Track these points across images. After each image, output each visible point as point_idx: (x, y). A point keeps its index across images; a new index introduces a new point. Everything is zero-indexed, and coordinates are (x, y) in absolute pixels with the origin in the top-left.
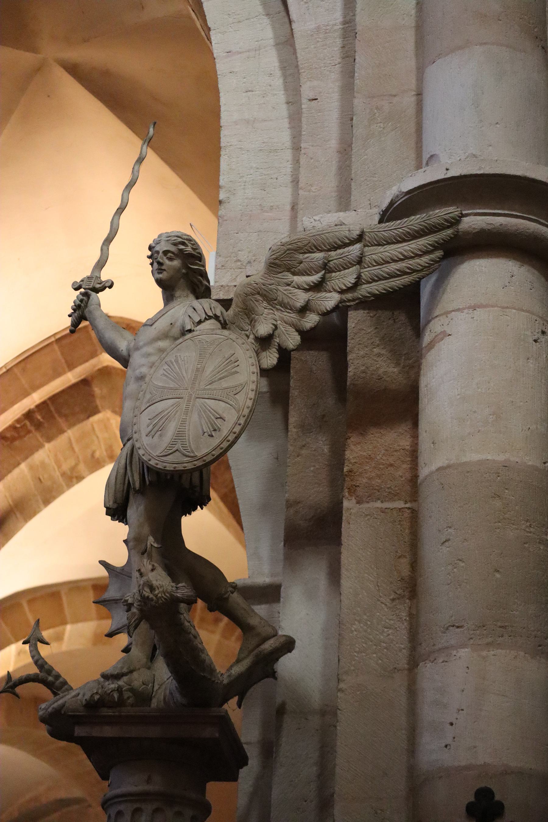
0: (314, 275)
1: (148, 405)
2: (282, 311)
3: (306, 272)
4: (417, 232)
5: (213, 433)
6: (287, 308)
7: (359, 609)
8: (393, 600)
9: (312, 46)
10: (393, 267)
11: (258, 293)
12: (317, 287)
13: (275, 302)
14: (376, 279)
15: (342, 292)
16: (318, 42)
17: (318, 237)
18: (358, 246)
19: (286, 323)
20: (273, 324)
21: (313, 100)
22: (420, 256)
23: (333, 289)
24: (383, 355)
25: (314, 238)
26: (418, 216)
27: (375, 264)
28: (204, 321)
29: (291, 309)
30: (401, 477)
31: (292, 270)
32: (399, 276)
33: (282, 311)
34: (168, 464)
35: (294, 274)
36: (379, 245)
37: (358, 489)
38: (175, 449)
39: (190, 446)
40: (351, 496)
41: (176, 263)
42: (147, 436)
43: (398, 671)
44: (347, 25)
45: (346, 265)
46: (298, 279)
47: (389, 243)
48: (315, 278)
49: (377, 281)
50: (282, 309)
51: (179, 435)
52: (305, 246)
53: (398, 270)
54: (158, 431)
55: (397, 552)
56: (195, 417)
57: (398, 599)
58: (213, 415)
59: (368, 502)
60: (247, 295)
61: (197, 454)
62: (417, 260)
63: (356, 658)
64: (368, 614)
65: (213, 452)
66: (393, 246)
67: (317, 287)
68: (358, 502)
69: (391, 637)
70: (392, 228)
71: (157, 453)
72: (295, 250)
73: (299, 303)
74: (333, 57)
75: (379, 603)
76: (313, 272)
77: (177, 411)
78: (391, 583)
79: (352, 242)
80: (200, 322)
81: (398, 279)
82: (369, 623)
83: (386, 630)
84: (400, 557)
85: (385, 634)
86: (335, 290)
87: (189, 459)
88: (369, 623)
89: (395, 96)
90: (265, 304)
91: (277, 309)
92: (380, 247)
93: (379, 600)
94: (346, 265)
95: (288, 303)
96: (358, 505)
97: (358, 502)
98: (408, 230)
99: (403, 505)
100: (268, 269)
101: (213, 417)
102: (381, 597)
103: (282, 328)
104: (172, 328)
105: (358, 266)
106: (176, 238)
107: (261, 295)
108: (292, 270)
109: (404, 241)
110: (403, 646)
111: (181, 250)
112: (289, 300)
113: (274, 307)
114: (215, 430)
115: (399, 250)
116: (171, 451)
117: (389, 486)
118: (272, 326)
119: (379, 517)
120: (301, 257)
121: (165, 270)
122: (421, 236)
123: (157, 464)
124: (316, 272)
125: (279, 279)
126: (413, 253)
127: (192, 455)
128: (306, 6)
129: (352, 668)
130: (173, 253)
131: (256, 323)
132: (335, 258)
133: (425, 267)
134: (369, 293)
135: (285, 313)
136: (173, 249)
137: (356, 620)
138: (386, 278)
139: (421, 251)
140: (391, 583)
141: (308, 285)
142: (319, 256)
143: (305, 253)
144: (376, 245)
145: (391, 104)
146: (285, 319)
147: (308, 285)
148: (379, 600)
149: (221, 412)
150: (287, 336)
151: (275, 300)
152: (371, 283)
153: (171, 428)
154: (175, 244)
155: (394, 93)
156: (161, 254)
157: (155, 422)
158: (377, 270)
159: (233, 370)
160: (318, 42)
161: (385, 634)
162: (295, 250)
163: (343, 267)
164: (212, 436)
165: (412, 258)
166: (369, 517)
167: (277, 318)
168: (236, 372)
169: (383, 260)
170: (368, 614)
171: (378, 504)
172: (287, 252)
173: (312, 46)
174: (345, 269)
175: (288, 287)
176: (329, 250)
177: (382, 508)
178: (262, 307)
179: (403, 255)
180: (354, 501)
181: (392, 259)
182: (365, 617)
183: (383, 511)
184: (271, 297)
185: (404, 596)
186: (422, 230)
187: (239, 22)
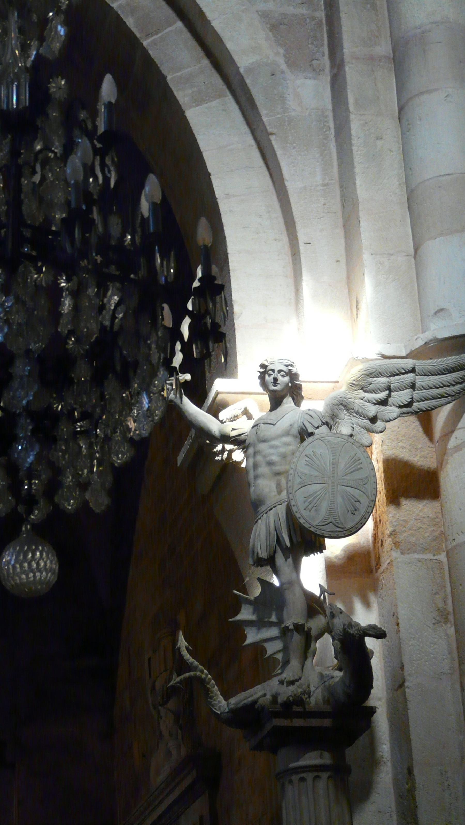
0: (379, 393)
1: (301, 486)
2: (357, 417)
3: (374, 391)
4: (452, 368)
5: (355, 512)
6: (361, 416)
7: (412, 630)
8: (434, 624)
9: (303, 201)
10: (435, 392)
11: (342, 404)
12: (383, 403)
13: (352, 411)
14: (424, 399)
15: (400, 407)
16: (306, 198)
17: (382, 366)
18: (411, 375)
19: (359, 426)
20: (352, 427)
21: (307, 243)
22: (453, 385)
23: (393, 404)
24: (405, 448)
25: (379, 367)
26: (453, 357)
27: (423, 389)
28: (321, 426)
29: (364, 417)
30: (429, 537)
31: (364, 389)
32: (439, 398)
33: (357, 417)
34: (325, 532)
35: (365, 391)
36: (425, 375)
37: (401, 544)
38: (328, 522)
39: (340, 521)
40: (397, 549)
41: (287, 379)
42: (305, 509)
43: (444, 674)
44: (325, 187)
45: (402, 388)
46: (367, 395)
47: (432, 375)
48: (382, 395)
49: (423, 401)
50: (357, 416)
51: (331, 511)
52: (374, 372)
53: (438, 394)
54: (313, 507)
55: (433, 590)
56: (340, 499)
57: (438, 623)
58: (353, 499)
59: (408, 554)
60: (334, 405)
61: (345, 526)
62: (452, 388)
63: (415, 665)
64: (419, 634)
65: (356, 526)
66: (435, 377)
67: (383, 403)
68: (402, 553)
69: (437, 650)
70: (435, 364)
71: (316, 523)
72: (367, 375)
73: (371, 414)
74: (318, 211)
75: (425, 626)
76: (379, 392)
77: (326, 494)
78: (432, 612)
79: (407, 372)
80: (318, 428)
81: (438, 400)
82: (420, 640)
83: (432, 645)
84: (435, 594)
85: (432, 648)
86: (394, 405)
87: (340, 529)
88: (420, 640)
89: (392, 255)
90: (345, 412)
91: (354, 416)
92: (426, 377)
93: (425, 624)
94: (402, 388)
95: (362, 412)
96: (402, 556)
97: (402, 553)
98: (447, 367)
99: (432, 557)
100: (348, 387)
101: (353, 501)
102: (426, 622)
103: (357, 429)
104: (291, 428)
105: (411, 389)
106: (286, 361)
107: (343, 406)
108: (364, 389)
109: (443, 374)
110: (445, 657)
111: (290, 371)
112: (363, 410)
113: (352, 415)
114: (356, 510)
115: (440, 380)
116: (326, 523)
117: (421, 543)
118: (351, 428)
119: (418, 565)
120: (371, 380)
121: (279, 384)
122: (455, 371)
123: (316, 531)
124: (381, 391)
125: (355, 395)
126: (449, 383)
127: (342, 526)
128: (295, 168)
129: (413, 672)
130: (285, 372)
131: (340, 426)
132: (394, 382)
133: (457, 393)
134: (419, 409)
135: (360, 419)
136: (285, 369)
137: (411, 638)
138: (430, 399)
139: (455, 382)
140: (432, 612)
141: (376, 400)
142: (383, 380)
143: (374, 377)
144: (423, 375)
145: (390, 261)
146: (360, 424)
147: (376, 400)
148: (425, 624)
149: (357, 497)
150: (362, 436)
151: (353, 410)
152: (419, 402)
153: (324, 507)
154: (287, 366)
155: (392, 253)
156: (276, 372)
157: (310, 500)
158: (424, 393)
159: (359, 467)
160: (306, 198)
161: (432, 648)
162: (367, 375)
163: (399, 389)
164: (354, 514)
165: (449, 386)
166: (410, 564)
167: (353, 422)
168: (361, 468)
169: (428, 386)
170: (419, 634)
171: (416, 556)
172: (362, 376)
173: (303, 201)
174: (401, 390)
175: (361, 401)
176: (390, 376)
177: (418, 559)
178: (343, 414)
179: (442, 384)
180: (399, 553)
181: (435, 386)
182: (417, 636)
183: (420, 560)
184: (349, 407)
185: (440, 622)
186: (456, 367)
187: (232, 171)
